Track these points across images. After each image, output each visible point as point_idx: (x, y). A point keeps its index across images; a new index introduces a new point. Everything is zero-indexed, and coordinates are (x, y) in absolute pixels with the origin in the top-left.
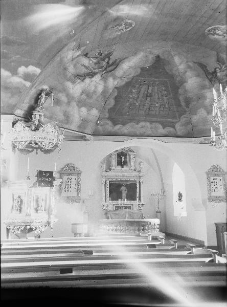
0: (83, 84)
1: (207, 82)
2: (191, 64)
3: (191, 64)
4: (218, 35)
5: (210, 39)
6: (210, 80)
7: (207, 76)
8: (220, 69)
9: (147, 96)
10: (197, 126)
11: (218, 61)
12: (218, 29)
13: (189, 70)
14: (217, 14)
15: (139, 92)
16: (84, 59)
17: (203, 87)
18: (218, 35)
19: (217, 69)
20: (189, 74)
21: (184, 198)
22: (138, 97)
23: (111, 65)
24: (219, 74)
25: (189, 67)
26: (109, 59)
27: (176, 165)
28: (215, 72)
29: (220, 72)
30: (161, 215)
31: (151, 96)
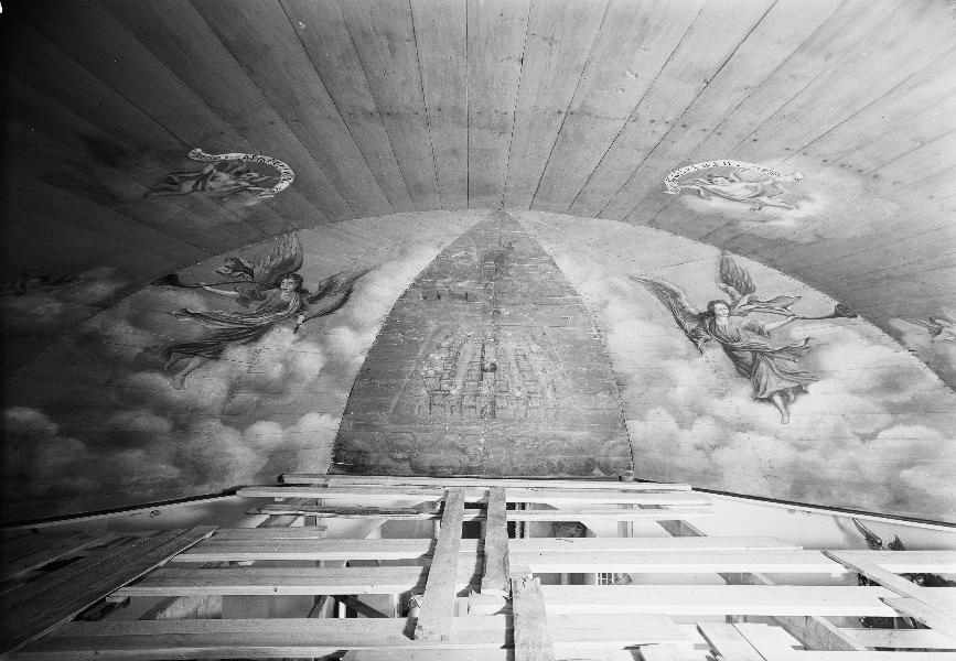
0: (220, 368)
1: (681, 341)
2: (624, 284)
3: (616, 281)
4: (731, 198)
5: (692, 212)
6: (693, 337)
7: (679, 322)
8: (729, 307)
9: (484, 370)
10: (647, 452)
11: (725, 282)
12: (726, 173)
13: (614, 299)
14: (720, 107)
15: (456, 359)
16: (172, 293)
17: (667, 353)
18: (731, 198)
19: (718, 306)
20: (616, 309)
21: (789, 146)
22: (453, 374)
23: (315, 299)
24: (722, 321)
25: (615, 290)
26: (299, 280)
27: (21, 303)
28: (711, 314)
29: (730, 315)
30: (392, 641)
31: (494, 368)
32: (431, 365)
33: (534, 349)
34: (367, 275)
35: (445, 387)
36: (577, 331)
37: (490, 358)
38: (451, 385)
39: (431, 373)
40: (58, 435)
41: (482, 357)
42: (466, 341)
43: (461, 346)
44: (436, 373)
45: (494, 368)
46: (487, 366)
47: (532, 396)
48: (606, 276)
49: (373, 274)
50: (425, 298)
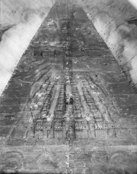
22: (49, 107)
32: (36, 102)
33: (93, 87)
34: (9, 31)
35: (44, 116)
36: (112, 70)
37: (69, 94)
38: (47, 115)
39: (36, 106)
40: (33, 11)
41: (65, 94)
42: (56, 84)
43: (53, 87)
44: (39, 106)
45: (72, 102)
46: (68, 100)
47: (97, 120)
48: (118, 27)
49: (10, 31)
50: (35, 55)
